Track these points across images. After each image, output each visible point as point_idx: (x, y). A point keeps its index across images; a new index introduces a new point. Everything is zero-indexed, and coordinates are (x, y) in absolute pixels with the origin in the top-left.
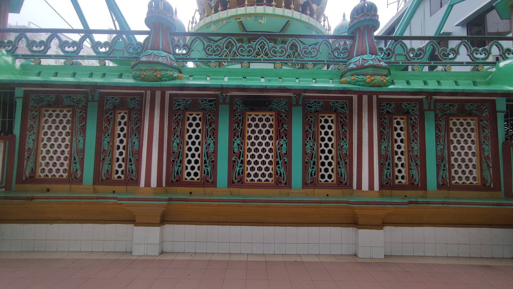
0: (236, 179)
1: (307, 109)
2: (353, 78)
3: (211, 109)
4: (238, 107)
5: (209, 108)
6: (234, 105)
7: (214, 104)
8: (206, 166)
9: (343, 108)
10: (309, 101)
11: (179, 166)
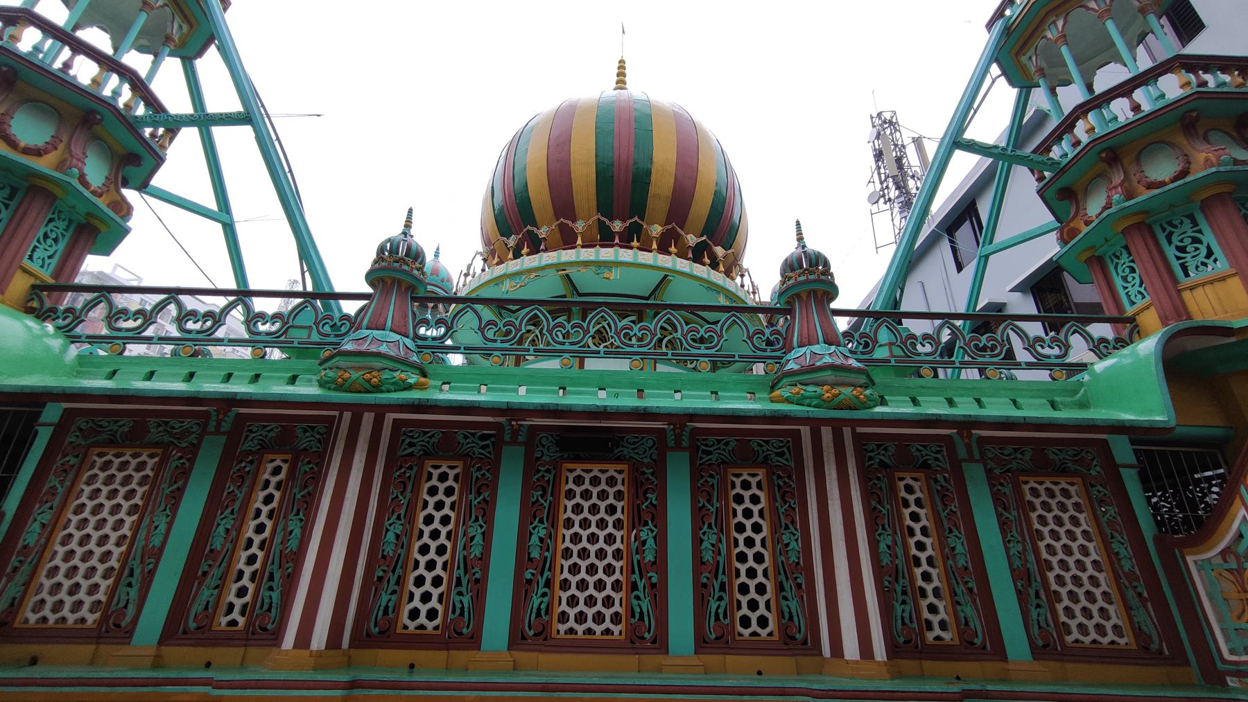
1: (701, 459)
2: (795, 390)
4: (546, 452)
5: (481, 454)
6: (538, 447)
9: (781, 454)
10: (704, 440)
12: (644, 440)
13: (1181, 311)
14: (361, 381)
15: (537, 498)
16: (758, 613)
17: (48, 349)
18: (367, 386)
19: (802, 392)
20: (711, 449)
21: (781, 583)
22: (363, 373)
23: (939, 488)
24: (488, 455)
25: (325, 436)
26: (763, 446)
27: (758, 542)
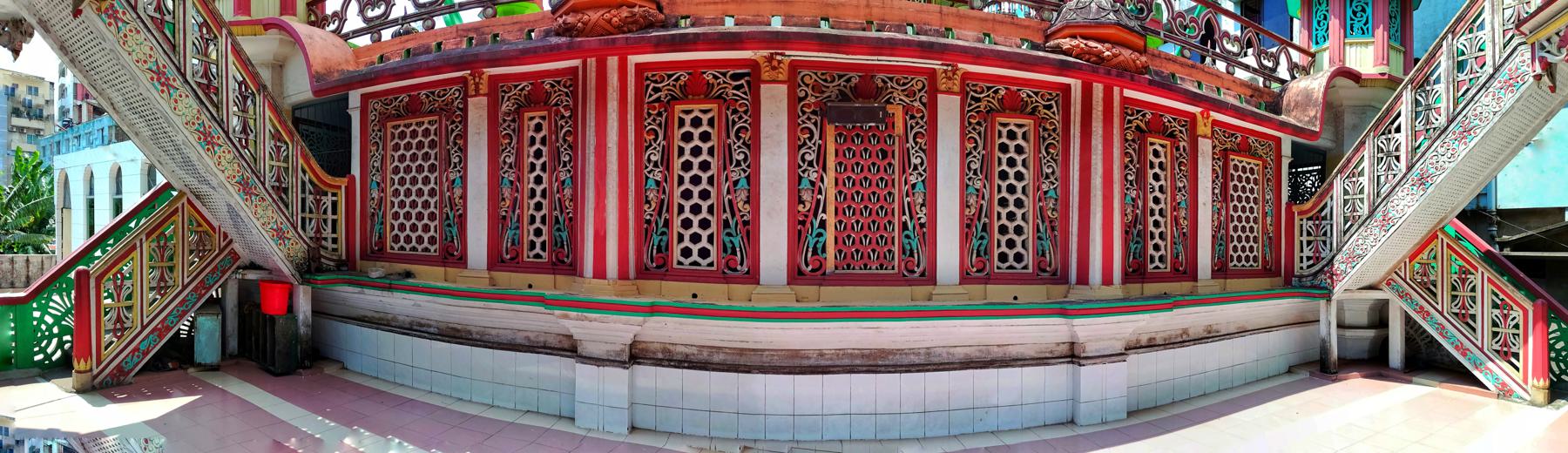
0: (807, 265)
1: (970, 105)
2: (1075, 42)
3: (739, 96)
4: (810, 92)
5: (734, 95)
6: (800, 86)
7: (745, 84)
8: (729, 235)
9: (1049, 107)
10: (973, 85)
11: (663, 233)
12: (914, 82)
13: (1342, 60)
14: (602, 22)
15: (805, 141)
16: (1015, 251)
17: (358, 52)
18: (608, 27)
19: (1082, 46)
20: (982, 96)
21: (1038, 225)
22: (601, 12)
23: (1178, 155)
24: (743, 96)
25: (571, 89)
26: (1032, 97)
27: (1019, 189)
